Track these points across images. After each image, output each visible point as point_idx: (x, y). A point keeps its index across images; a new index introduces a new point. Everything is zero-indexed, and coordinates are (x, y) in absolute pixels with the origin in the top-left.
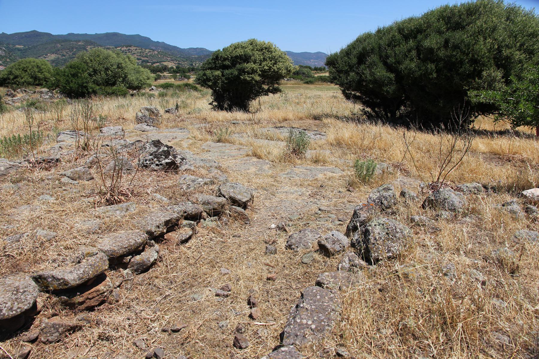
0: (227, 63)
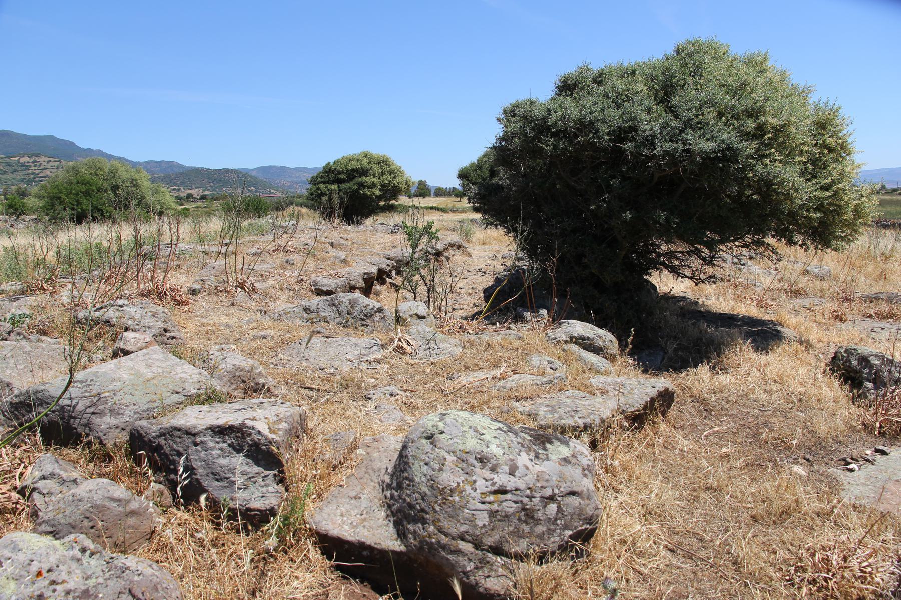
0: (342, 177)
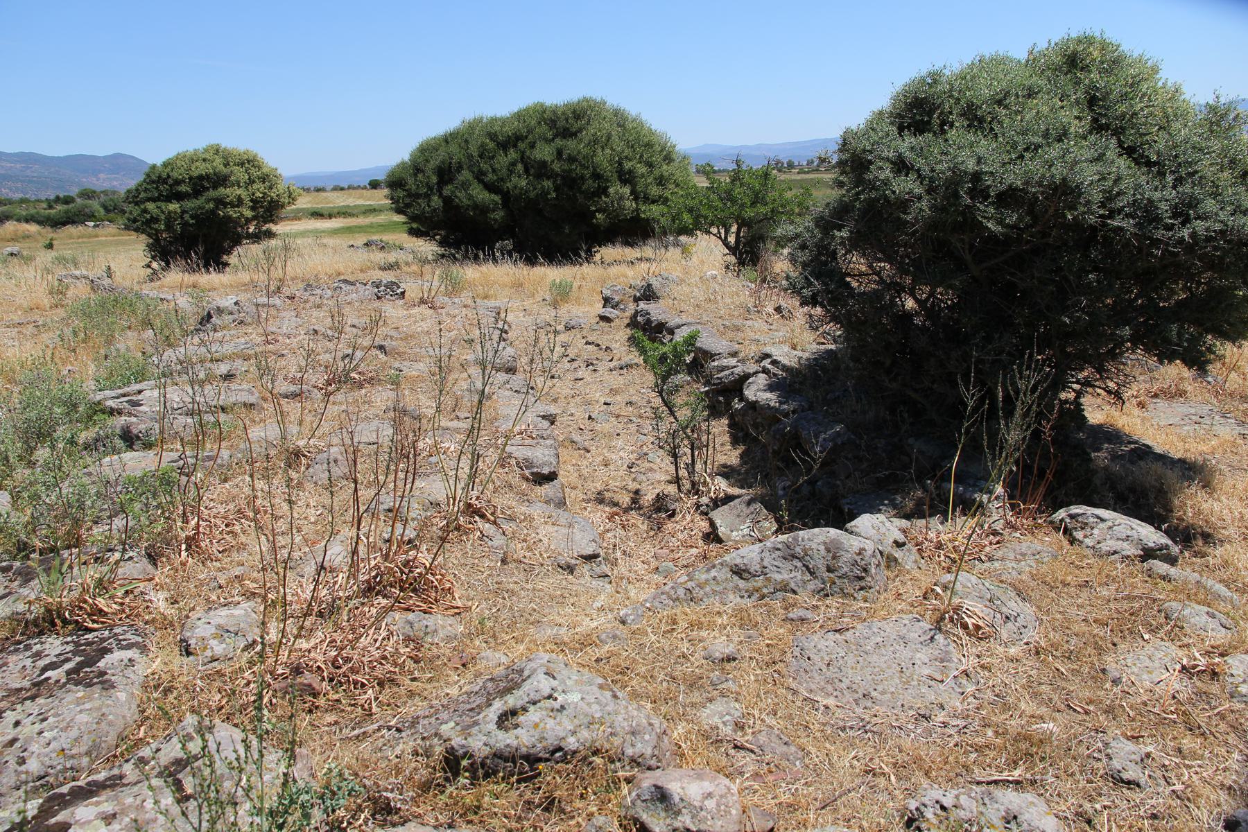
0: (183, 188)
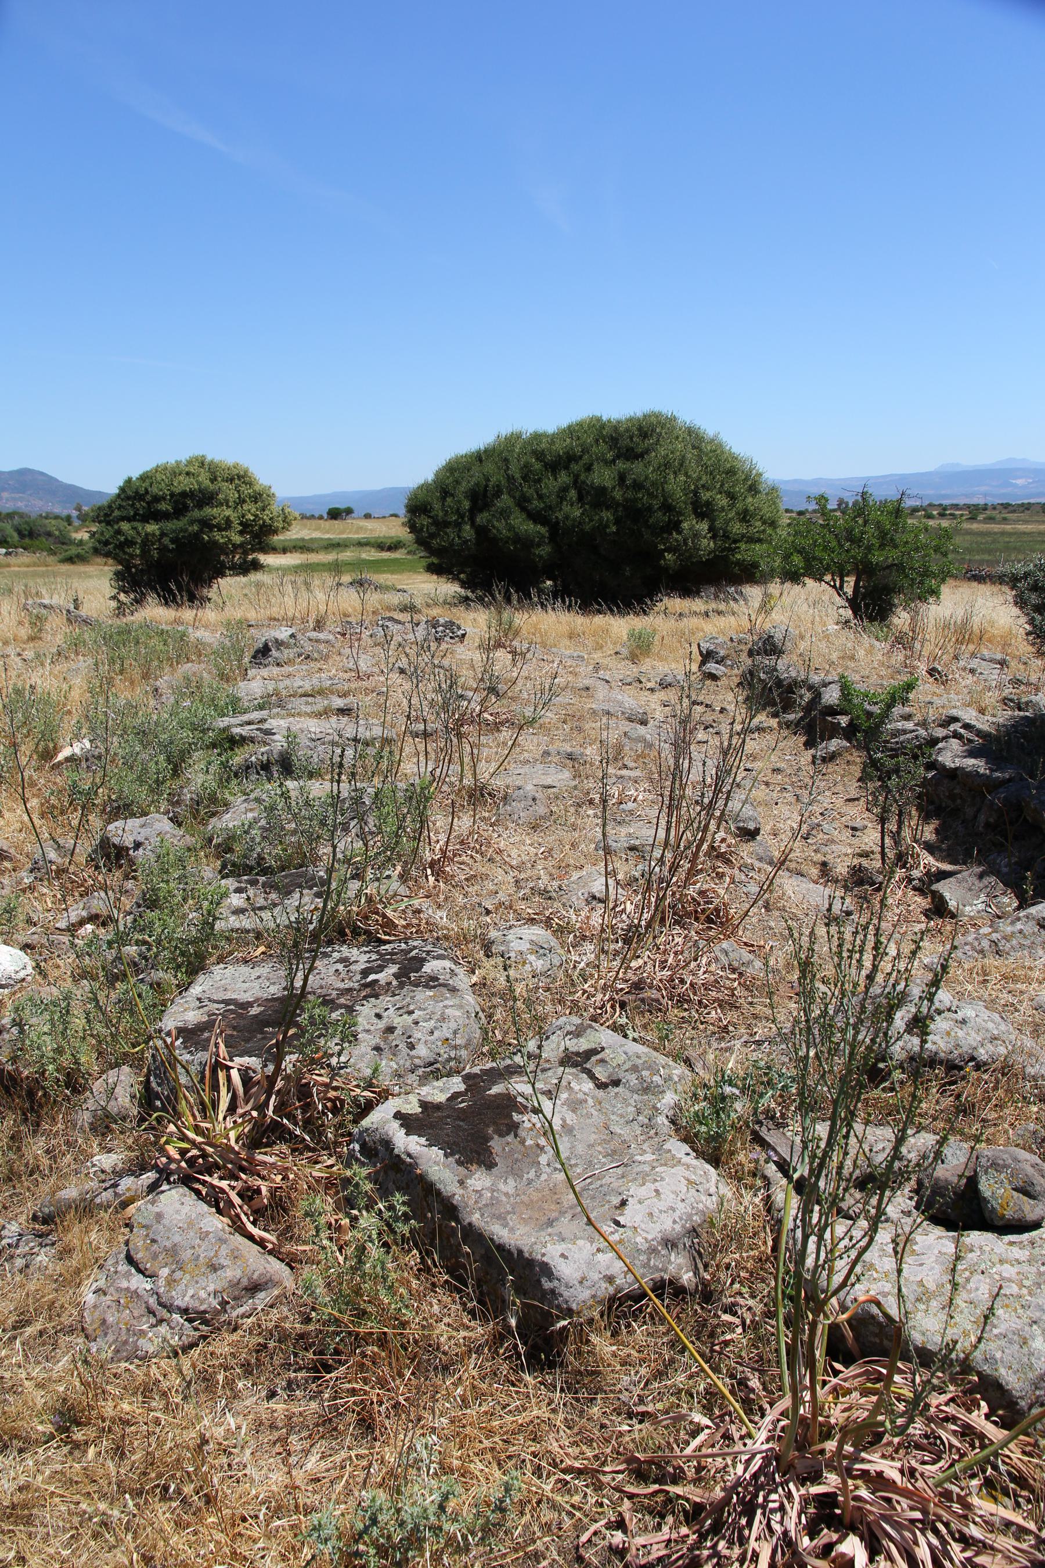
0: (163, 506)
